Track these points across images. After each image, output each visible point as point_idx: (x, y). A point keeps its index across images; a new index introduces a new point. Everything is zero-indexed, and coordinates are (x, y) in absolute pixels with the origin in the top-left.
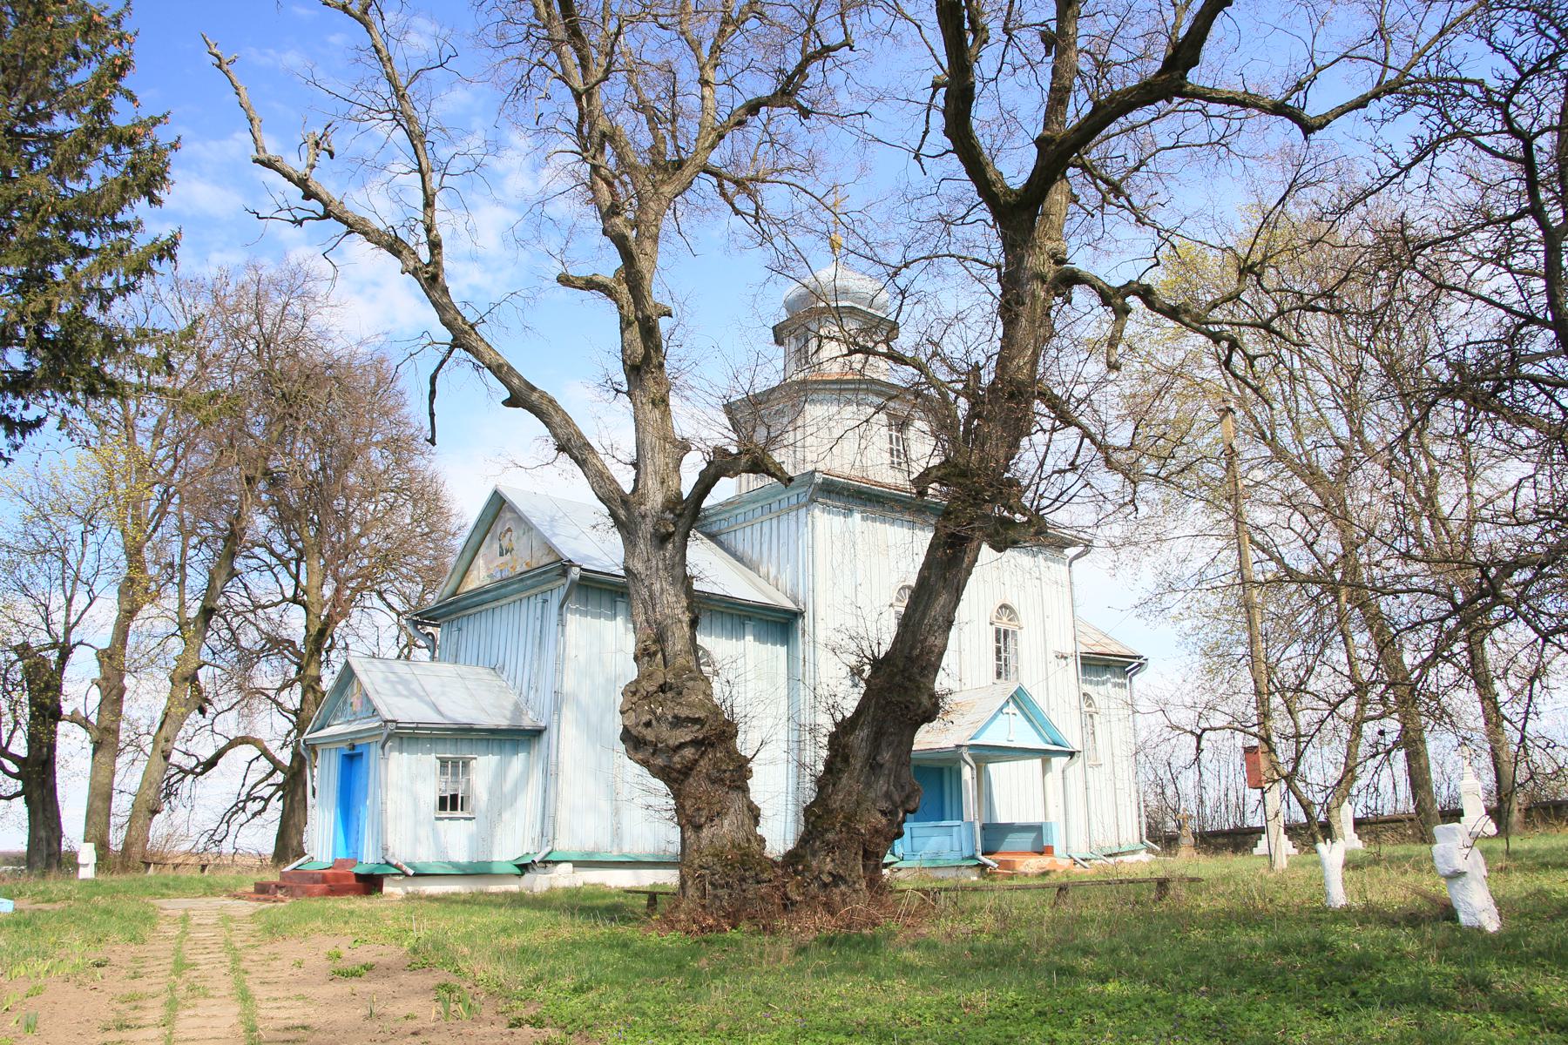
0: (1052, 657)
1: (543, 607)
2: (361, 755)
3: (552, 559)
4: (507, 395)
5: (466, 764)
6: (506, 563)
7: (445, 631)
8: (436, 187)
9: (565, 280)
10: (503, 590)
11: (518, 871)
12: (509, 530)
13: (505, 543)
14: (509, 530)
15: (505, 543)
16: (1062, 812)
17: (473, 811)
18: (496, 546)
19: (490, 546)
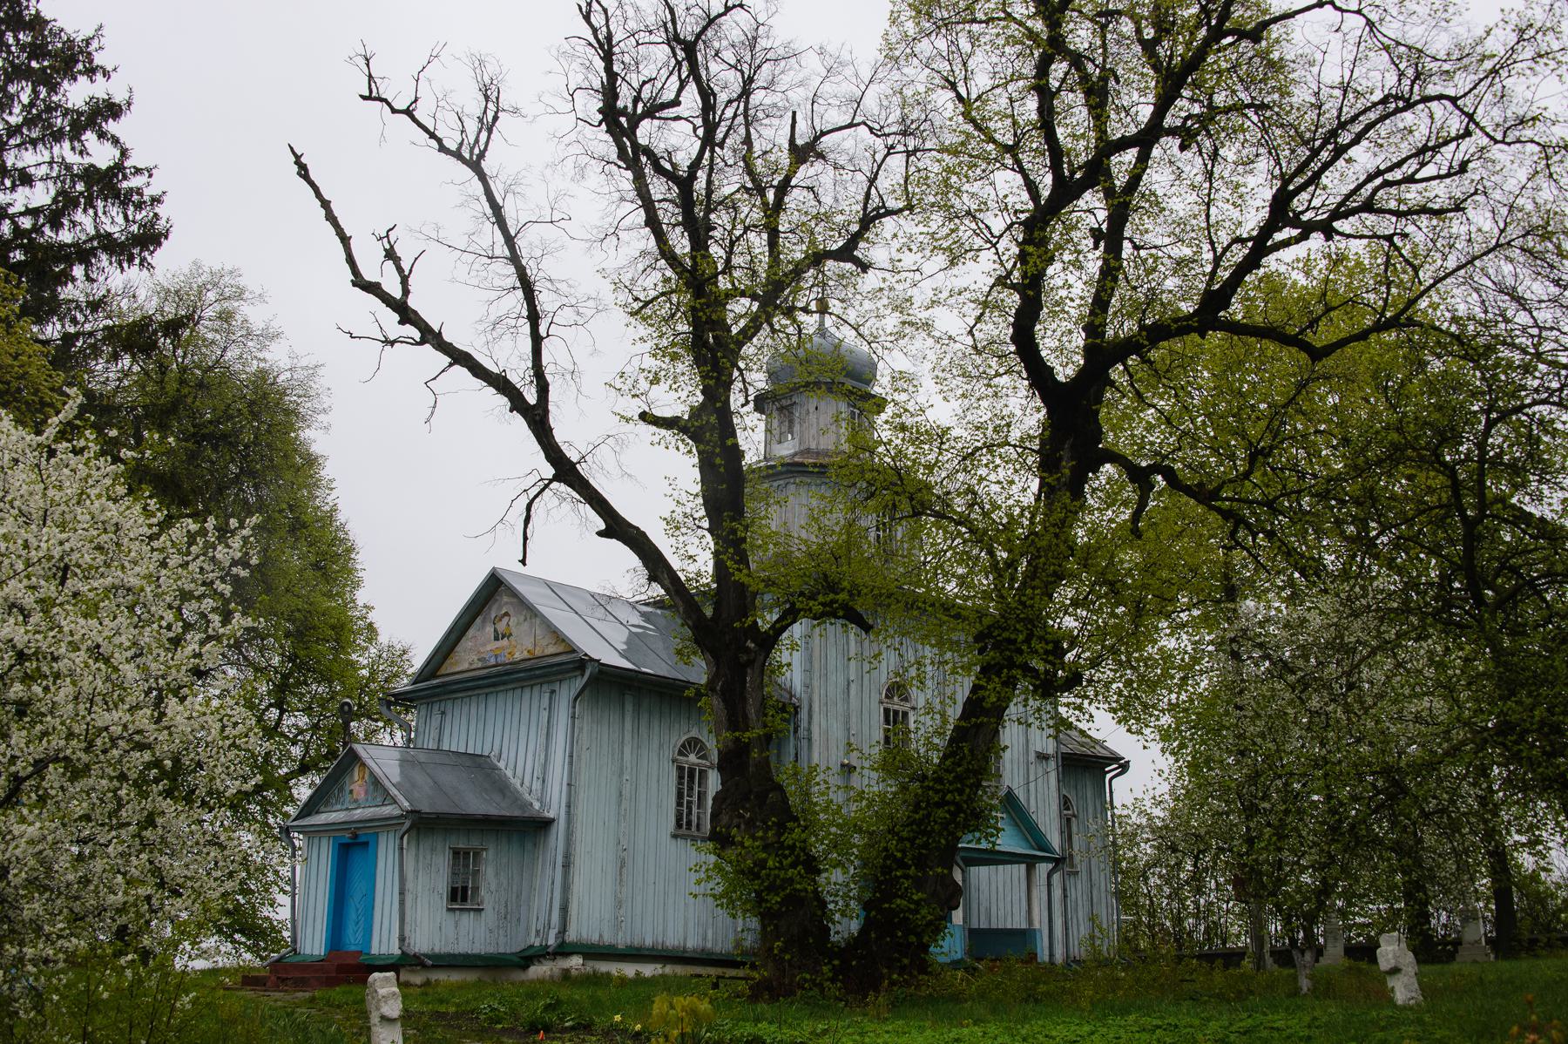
0: (1032, 757)
1: (550, 698)
2: (366, 844)
3: (560, 649)
4: (602, 526)
5: (477, 854)
6: (503, 648)
7: (423, 712)
8: (544, 335)
9: (645, 417)
10: (505, 678)
11: (522, 962)
12: (506, 614)
13: (501, 626)
14: (506, 614)
15: (501, 626)
16: (408, 919)
17: (482, 903)
18: (490, 629)
19: (480, 629)
